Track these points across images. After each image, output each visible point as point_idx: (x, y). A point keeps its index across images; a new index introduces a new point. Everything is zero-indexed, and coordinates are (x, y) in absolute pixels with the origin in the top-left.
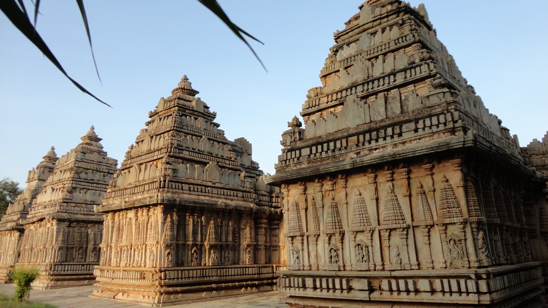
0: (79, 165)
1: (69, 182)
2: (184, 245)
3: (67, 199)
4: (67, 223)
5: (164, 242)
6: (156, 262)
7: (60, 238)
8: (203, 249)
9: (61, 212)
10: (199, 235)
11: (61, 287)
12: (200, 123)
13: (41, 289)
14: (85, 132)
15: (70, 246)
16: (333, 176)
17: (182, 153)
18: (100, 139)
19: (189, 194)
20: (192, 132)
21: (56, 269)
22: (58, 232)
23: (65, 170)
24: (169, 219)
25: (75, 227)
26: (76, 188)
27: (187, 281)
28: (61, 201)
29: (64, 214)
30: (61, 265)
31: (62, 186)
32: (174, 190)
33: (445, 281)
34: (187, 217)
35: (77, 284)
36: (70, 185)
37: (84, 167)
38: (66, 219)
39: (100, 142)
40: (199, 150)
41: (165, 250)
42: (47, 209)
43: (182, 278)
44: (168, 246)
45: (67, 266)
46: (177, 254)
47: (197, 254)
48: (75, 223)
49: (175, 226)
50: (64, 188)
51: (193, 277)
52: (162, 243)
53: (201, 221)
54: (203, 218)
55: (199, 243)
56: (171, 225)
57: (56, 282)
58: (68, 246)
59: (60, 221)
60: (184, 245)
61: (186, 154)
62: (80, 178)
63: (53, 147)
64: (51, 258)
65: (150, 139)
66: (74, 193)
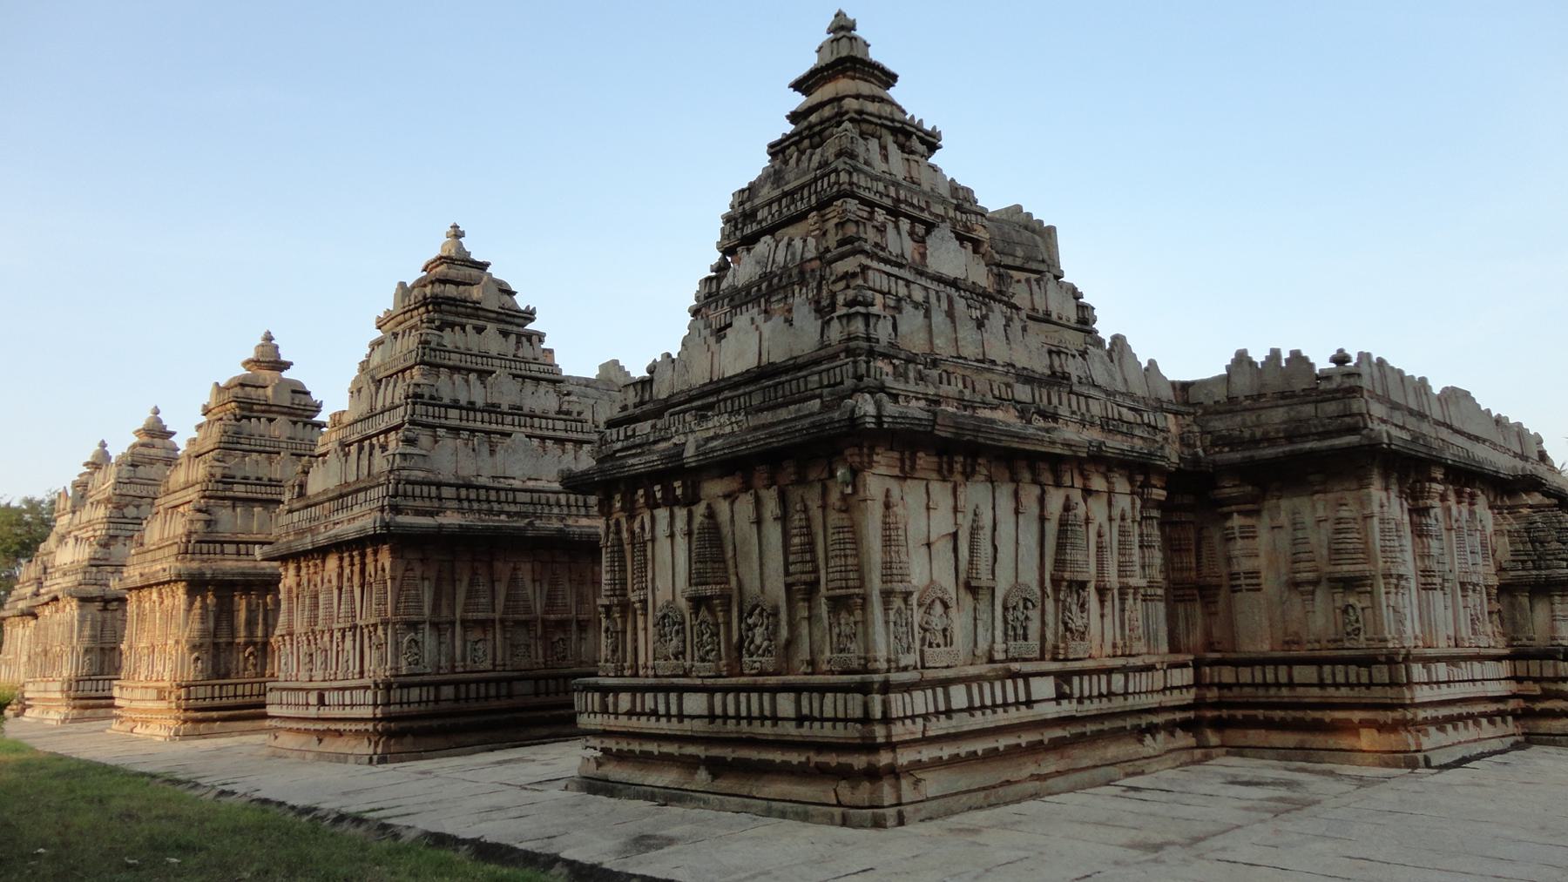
0: (124, 491)
1: (102, 526)
2: (230, 644)
3: (98, 559)
4: (99, 605)
5: (187, 641)
6: (176, 673)
7: (87, 632)
8: (269, 649)
9: (85, 584)
10: (260, 627)
11: (90, 719)
12: (281, 428)
13: (55, 723)
14: (141, 420)
15: (107, 646)
16: (307, 554)
17: (231, 490)
18: (173, 434)
19: (237, 560)
20: (257, 448)
21: (81, 688)
22: (82, 621)
23: (98, 502)
24: (198, 604)
25: (116, 610)
26: (117, 536)
27: (232, 701)
28: (86, 563)
29: (91, 588)
30: (90, 680)
31: (90, 533)
32: (206, 556)
33: (661, 697)
34: (236, 599)
35: (249, 728)
36: (104, 532)
37: (134, 494)
38: (96, 597)
39: (173, 439)
40: (270, 480)
41: (191, 653)
42: (67, 579)
43: (221, 698)
44: (194, 648)
45: (101, 682)
46: (216, 657)
47: (255, 658)
48: (115, 603)
49: (211, 614)
50: (94, 537)
51: (244, 696)
52: (184, 642)
53: (265, 604)
54: (269, 597)
55: (259, 640)
56: (202, 614)
57: (82, 711)
58: (103, 646)
59: (84, 600)
60: (230, 644)
61: (239, 491)
62: (124, 517)
63: (103, 441)
64: (71, 669)
65: (373, 389)
66: (112, 548)
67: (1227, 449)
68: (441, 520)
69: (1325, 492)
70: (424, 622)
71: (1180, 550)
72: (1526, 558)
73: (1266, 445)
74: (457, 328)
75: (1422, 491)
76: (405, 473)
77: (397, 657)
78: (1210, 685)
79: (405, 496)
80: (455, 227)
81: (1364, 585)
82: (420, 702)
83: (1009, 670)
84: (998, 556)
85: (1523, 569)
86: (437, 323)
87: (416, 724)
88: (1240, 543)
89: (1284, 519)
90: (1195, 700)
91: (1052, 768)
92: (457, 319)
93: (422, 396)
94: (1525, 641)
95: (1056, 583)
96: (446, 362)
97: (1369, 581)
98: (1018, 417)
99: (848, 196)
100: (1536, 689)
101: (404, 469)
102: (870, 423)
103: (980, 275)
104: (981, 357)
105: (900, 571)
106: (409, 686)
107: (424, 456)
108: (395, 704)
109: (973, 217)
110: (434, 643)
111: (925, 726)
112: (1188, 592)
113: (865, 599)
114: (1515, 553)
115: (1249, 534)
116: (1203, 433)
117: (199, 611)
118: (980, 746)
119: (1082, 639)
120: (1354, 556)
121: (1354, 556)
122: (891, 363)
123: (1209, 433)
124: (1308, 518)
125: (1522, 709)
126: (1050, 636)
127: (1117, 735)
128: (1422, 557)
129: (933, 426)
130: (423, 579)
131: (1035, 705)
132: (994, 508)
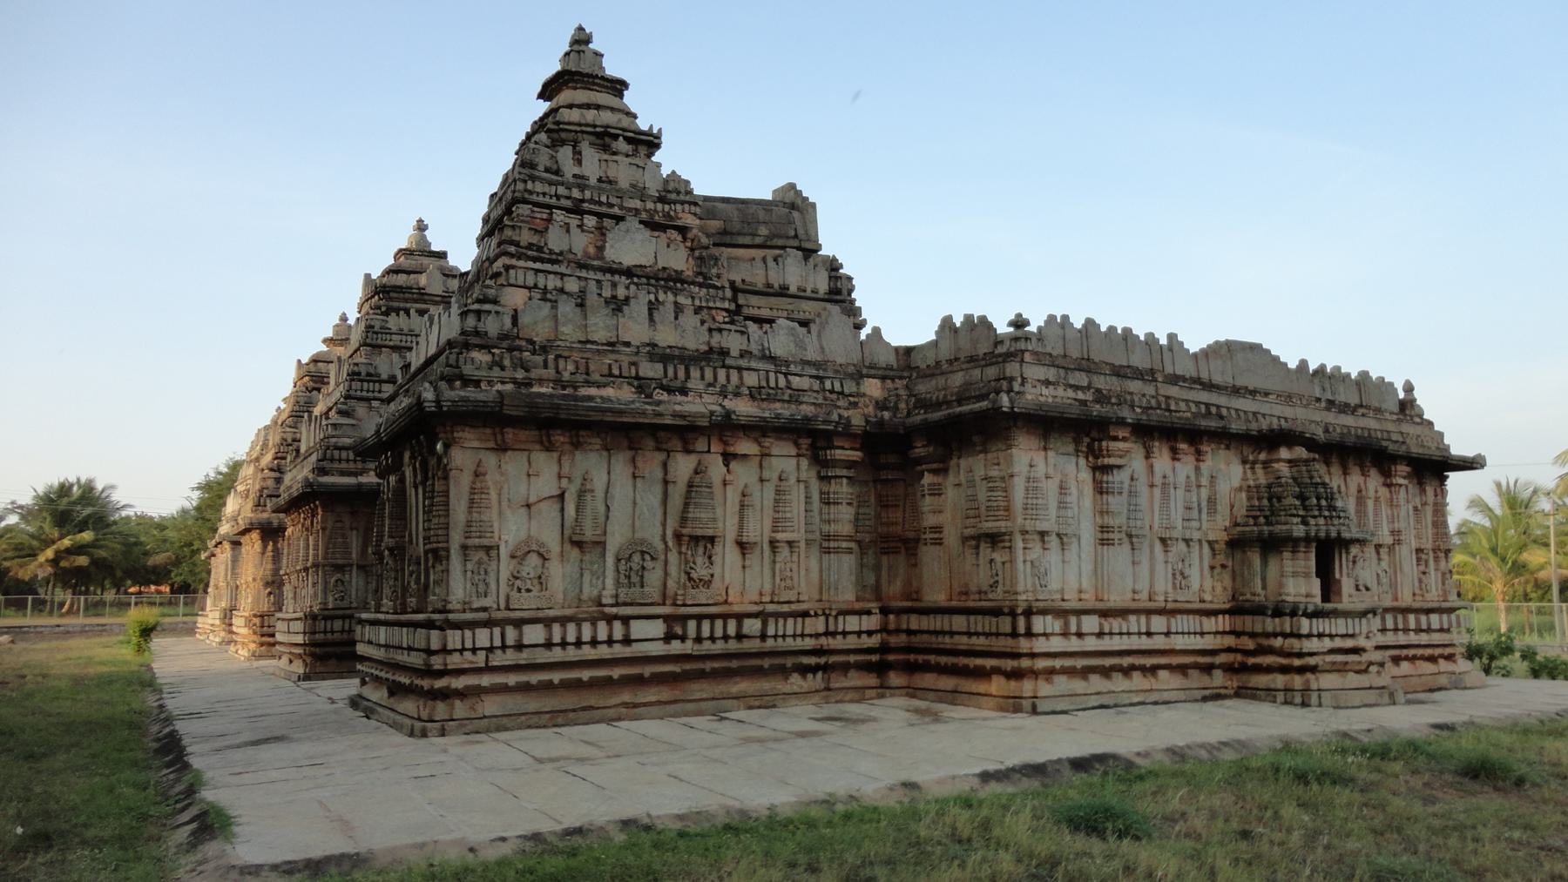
24: (270, 548)
56: (273, 556)
67: (922, 411)
68: (363, 479)
69: (985, 451)
70: (351, 565)
71: (887, 506)
72: (1258, 513)
73: (1198, 387)
74: (402, 313)
75: (1101, 450)
76: (334, 440)
77: (326, 594)
78: (898, 631)
79: (332, 460)
80: (420, 221)
81: (1003, 541)
82: (325, 632)
83: (603, 613)
84: (610, 514)
85: (1255, 525)
86: (383, 309)
87: (338, 650)
88: (928, 499)
89: (962, 478)
90: (881, 644)
91: (653, 698)
92: (402, 305)
93: (359, 374)
94: (1248, 596)
95: (678, 537)
96: (387, 343)
97: (1007, 537)
98: (636, 393)
99: (520, 202)
100: (1250, 644)
101: (333, 437)
102: (430, 407)
103: (678, 259)
104: (614, 339)
105: (1034, 512)
106: (333, 618)
107: (353, 425)
108: (320, 632)
109: (679, 207)
110: (361, 583)
111: (487, 657)
112: (892, 545)
113: (447, 550)
114: (1251, 508)
115: (937, 491)
116: (910, 396)
117: (271, 554)
118: (556, 677)
119: (708, 588)
120: (996, 513)
121: (996, 513)
122: (490, 352)
123: (915, 396)
124: (1041, 470)
125: (1239, 663)
126: (671, 583)
127: (758, 672)
128: (1102, 513)
129: (501, 407)
130: (352, 529)
131: (634, 644)
132: (609, 473)
